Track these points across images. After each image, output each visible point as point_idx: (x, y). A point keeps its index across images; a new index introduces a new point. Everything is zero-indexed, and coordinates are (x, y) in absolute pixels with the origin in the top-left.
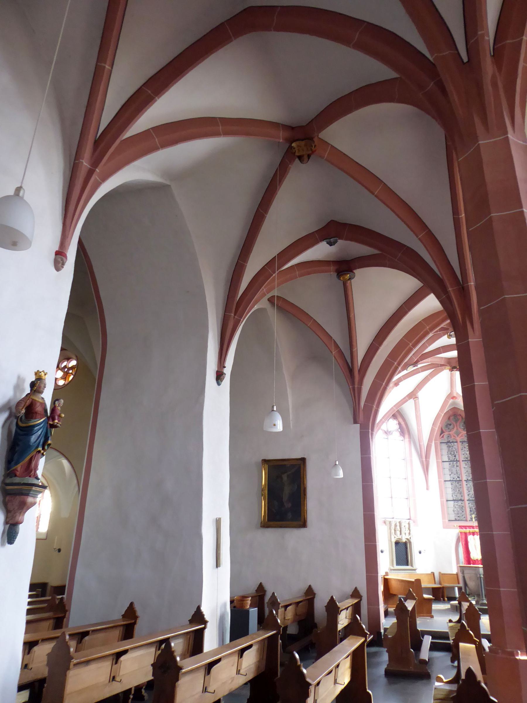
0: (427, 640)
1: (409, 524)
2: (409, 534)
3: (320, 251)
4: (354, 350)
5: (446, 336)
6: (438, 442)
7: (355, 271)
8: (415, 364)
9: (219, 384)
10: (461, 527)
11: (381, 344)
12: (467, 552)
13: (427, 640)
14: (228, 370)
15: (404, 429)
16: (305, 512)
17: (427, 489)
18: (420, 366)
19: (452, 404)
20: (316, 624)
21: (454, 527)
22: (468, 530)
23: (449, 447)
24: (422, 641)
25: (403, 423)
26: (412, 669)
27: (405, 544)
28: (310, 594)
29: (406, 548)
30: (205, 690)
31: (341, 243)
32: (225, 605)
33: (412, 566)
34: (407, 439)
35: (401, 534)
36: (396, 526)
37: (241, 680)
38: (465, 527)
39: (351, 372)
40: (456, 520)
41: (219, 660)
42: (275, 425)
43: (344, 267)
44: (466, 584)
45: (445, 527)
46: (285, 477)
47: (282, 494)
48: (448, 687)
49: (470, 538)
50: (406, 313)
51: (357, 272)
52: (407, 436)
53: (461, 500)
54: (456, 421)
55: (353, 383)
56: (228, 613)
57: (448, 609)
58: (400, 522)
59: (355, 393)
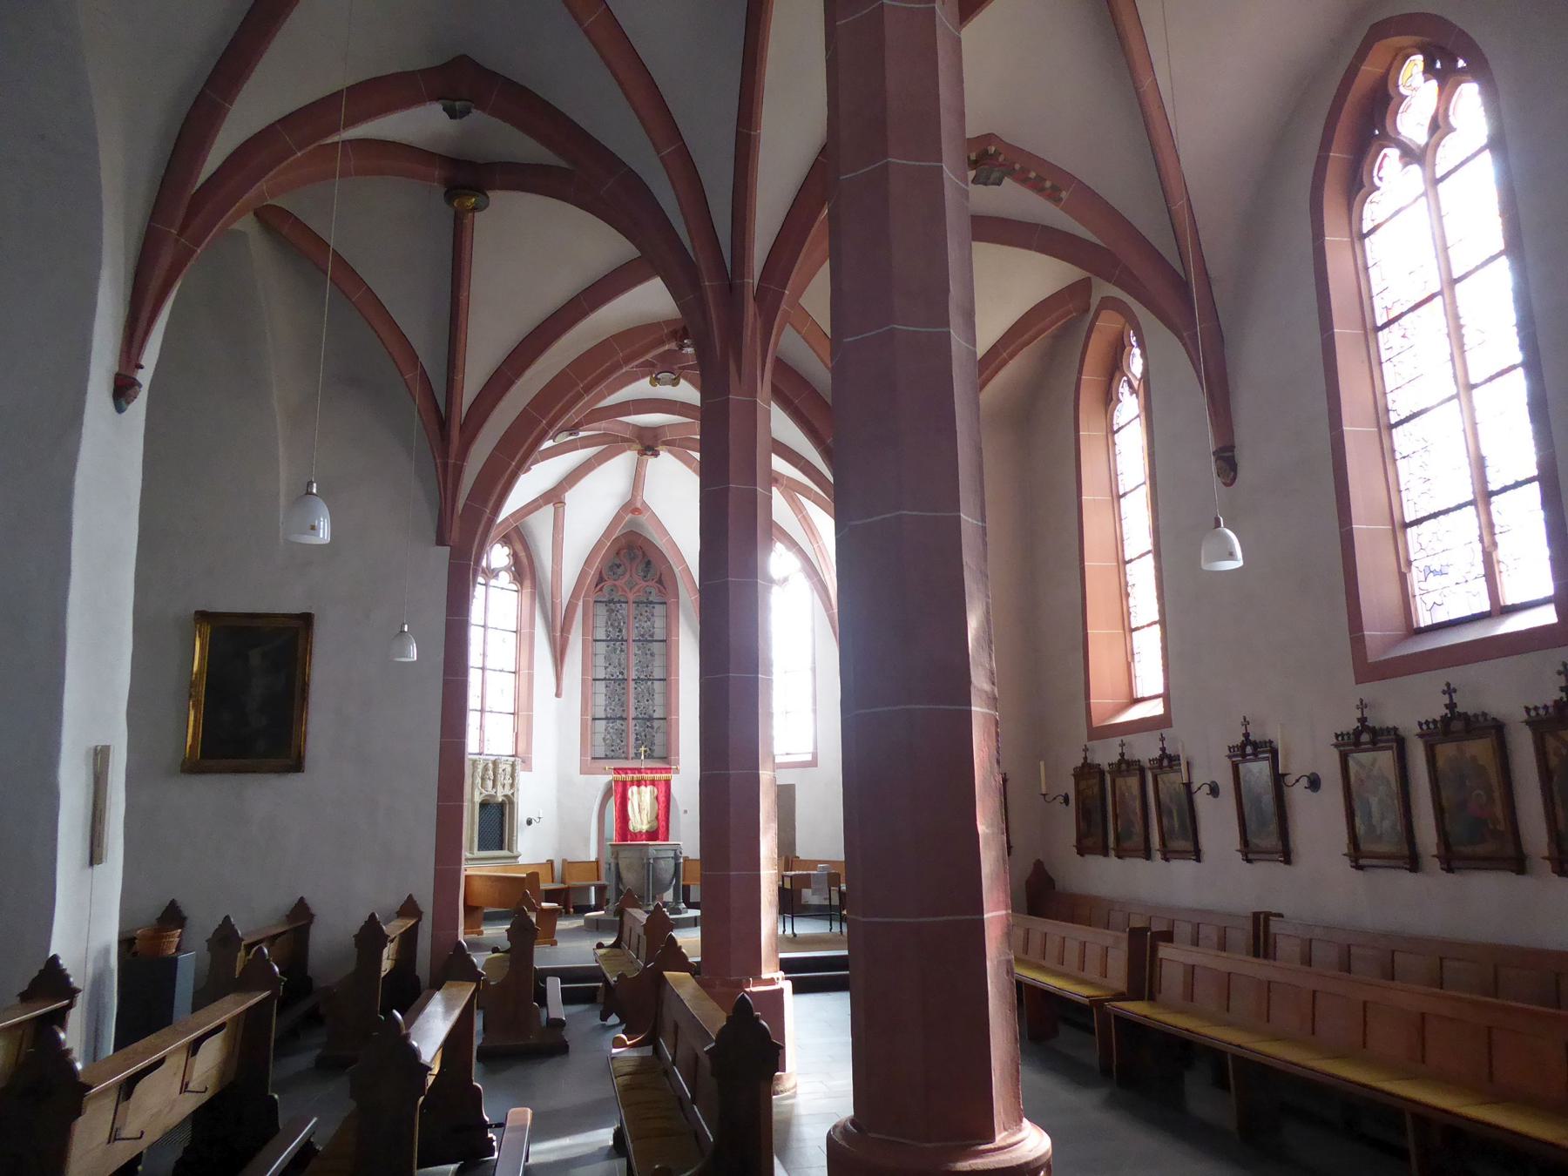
0: (554, 986)
1: (513, 765)
2: (512, 785)
3: (421, 124)
4: (458, 378)
5: (648, 379)
6: (591, 600)
7: (490, 194)
8: (573, 429)
9: (120, 409)
10: (617, 771)
11: (519, 373)
12: (623, 817)
13: (554, 986)
14: (145, 377)
15: (524, 570)
16: (303, 736)
17: (558, 695)
18: (582, 434)
19: (630, 522)
20: (310, 980)
21: (604, 772)
22: (629, 777)
23: (611, 611)
24: (545, 990)
25: (522, 554)
26: (533, 1039)
27: (502, 805)
28: (301, 915)
29: (503, 815)
30: (114, 1137)
31: (478, 118)
32: (107, 951)
33: (510, 849)
34: (527, 590)
35: (494, 786)
36: (486, 769)
37: (190, 1104)
38: (625, 771)
39: (445, 431)
40: (606, 757)
41: (161, 1062)
42: (313, 528)
43: (466, 179)
44: (619, 877)
45: (584, 770)
46: (255, 658)
47: (243, 693)
48: (634, 1054)
49: (633, 791)
50: (584, 314)
51: (495, 196)
52: (527, 583)
53: (621, 718)
54: (632, 559)
55: (445, 453)
56: (111, 972)
57: (579, 929)
58: (495, 763)
59: (448, 475)
